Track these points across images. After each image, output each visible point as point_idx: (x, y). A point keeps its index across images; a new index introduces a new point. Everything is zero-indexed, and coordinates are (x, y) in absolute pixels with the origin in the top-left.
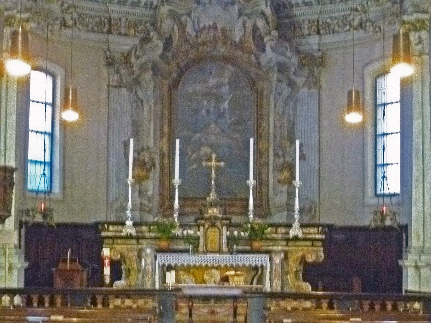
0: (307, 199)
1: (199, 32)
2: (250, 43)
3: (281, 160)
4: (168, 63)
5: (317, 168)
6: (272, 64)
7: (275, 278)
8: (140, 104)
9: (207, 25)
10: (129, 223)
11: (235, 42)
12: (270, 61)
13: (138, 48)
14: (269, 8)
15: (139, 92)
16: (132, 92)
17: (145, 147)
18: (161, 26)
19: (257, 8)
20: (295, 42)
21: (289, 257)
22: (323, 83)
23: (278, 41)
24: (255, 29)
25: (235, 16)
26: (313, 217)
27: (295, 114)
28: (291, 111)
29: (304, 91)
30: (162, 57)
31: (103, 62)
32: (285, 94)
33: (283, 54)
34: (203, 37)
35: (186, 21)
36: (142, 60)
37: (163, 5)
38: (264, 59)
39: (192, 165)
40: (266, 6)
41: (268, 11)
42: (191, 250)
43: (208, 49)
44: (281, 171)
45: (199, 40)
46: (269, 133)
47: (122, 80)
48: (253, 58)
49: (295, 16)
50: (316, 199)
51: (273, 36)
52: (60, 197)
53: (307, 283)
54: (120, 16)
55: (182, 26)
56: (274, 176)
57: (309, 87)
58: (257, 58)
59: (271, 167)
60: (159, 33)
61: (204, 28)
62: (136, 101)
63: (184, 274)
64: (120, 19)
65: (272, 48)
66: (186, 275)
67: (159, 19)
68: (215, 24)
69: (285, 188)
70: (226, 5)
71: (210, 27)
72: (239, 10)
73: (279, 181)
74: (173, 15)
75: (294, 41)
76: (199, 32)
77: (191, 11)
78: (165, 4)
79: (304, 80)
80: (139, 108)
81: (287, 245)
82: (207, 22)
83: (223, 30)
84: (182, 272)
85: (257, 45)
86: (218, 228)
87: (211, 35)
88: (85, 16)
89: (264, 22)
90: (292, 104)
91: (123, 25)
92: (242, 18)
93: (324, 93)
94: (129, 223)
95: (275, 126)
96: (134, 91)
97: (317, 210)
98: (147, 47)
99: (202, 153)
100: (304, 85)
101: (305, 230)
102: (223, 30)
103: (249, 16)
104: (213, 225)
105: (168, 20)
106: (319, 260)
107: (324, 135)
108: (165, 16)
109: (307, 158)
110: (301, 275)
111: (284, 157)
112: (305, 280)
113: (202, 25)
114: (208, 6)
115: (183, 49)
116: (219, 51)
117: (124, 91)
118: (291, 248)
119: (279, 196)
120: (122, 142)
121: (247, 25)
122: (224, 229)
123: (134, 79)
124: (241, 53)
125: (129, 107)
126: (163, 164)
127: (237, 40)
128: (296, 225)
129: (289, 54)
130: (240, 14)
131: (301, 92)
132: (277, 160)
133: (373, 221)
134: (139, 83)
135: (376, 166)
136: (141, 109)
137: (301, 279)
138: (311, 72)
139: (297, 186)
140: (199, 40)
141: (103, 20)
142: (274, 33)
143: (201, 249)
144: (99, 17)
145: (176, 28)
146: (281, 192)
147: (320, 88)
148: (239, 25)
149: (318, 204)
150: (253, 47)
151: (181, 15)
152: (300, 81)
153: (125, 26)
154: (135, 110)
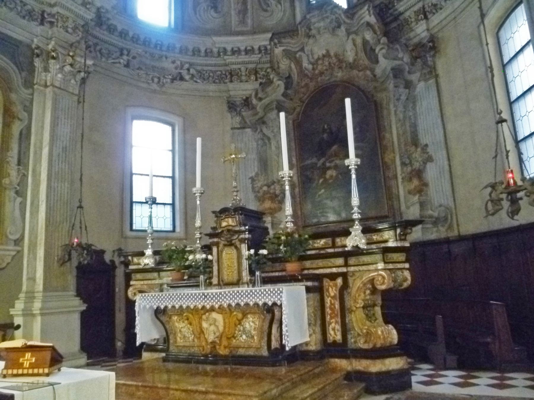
0: (441, 206)
1: (314, 64)
2: (364, 61)
3: (409, 169)
4: (291, 99)
5: (447, 167)
6: (387, 73)
7: (332, 321)
8: (267, 141)
9: (321, 54)
10: (149, 252)
11: (350, 64)
12: (384, 70)
13: (259, 91)
14: (373, 16)
15: (265, 130)
16: (257, 130)
17: (275, 180)
18: (278, 68)
19: (362, 22)
20: (403, 41)
21: (351, 285)
22: (440, 71)
23: (388, 46)
24: (365, 43)
25: (345, 39)
26: (450, 227)
27: (415, 115)
28: (411, 114)
29: (421, 86)
30: (285, 95)
31: (225, 107)
32: (403, 98)
33: (396, 58)
34: (320, 67)
35: (300, 56)
36: (266, 101)
37: (276, 47)
38: (378, 71)
39: (320, 190)
40: (370, 16)
41: (372, 20)
42: (258, 280)
43: (325, 78)
44: (410, 180)
45: (317, 72)
46: (393, 142)
47: (246, 122)
48: (368, 72)
49: (401, 14)
50: (452, 204)
51: (383, 44)
52: (182, 235)
53: (391, 327)
54: (239, 66)
55: (298, 63)
56: (404, 187)
57: (426, 80)
58: (372, 71)
59: (400, 180)
60: (278, 74)
61: (319, 59)
62: (262, 139)
63: (178, 320)
64: (240, 69)
65: (385, 57)
66: (181, 322)
67: (275, 60)
68: (328, 51)
69: (416, 198)
70: (334, 29)
71: (324, 56)
72: (346, 31)
73: (410, 192)
74: (288, 54)
75: (402, 40)
76: (314, 64)
77: (303, 47)
78: (278, 45)
79: (418, 74)
80: (266, 145)
81: (346, 265)
82: (319, 52)
83: (336, 55)
84: (176, 317)
85: (370, 59)
86: (236, 247)
87: (327, 63)
88: (205, 72)
89: (372, 32)
90: (411, 105)
91: (244, 74)
92: (351, 37)
93: (443, 81)
94: (149, 252)
95: (398, 135)
96: (259, 130)
97: (454, 217)
98: (269, 89)
99: (328, 176)
100: (419, 81)
101: (368, 235)
102: (336, 55)
103: (356, 33)
104: (230, 244)
105: (285, 60)
106: (401, 285)
107: (449, 127)
108: (280, 58)
109: (434, 157)
110: (378, 310)
111: (411, 164)
112: (387, 321)
113: (316, 57)
114: (318, 37)
115: (303, 84)
116: (337, 77)
117: (248, 130)
118: (352, 269)
119: (412, 209)
120: (250, 178)
121: (357, 43)
122: (244, 248)
123: (259, 119)
124: (357, 72)
125: (255, 144)
126: (294, 193)
127: (351, 60)
128: (357, 228)
129: (400, 55)
130: (348, 33)
131: (418, 90)
132: (405, 169)
133: (490, 203)
134: (264, 123)
135: (517, 143)
136: (268, 146)
137: (380, 319)
138: (425, 63)
139: (353, 167)
140: (317, 72)
141: (224, 73)
142: (384, 40)
143: (215, 281)
144: (220, 71)
145: (293, 66)
146: (413, 204)
147: (437, 76)
148: (349, 46)
149: (454, 212)
150: (366, 62)
151: (296, 53)
152: (414, 77)
153: (246, 75)
154: (262, 146)
